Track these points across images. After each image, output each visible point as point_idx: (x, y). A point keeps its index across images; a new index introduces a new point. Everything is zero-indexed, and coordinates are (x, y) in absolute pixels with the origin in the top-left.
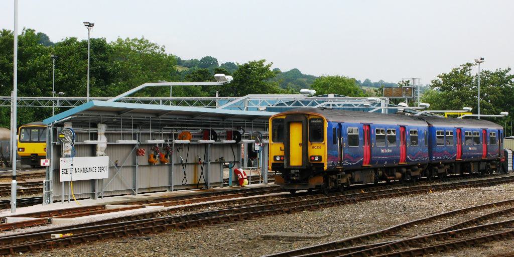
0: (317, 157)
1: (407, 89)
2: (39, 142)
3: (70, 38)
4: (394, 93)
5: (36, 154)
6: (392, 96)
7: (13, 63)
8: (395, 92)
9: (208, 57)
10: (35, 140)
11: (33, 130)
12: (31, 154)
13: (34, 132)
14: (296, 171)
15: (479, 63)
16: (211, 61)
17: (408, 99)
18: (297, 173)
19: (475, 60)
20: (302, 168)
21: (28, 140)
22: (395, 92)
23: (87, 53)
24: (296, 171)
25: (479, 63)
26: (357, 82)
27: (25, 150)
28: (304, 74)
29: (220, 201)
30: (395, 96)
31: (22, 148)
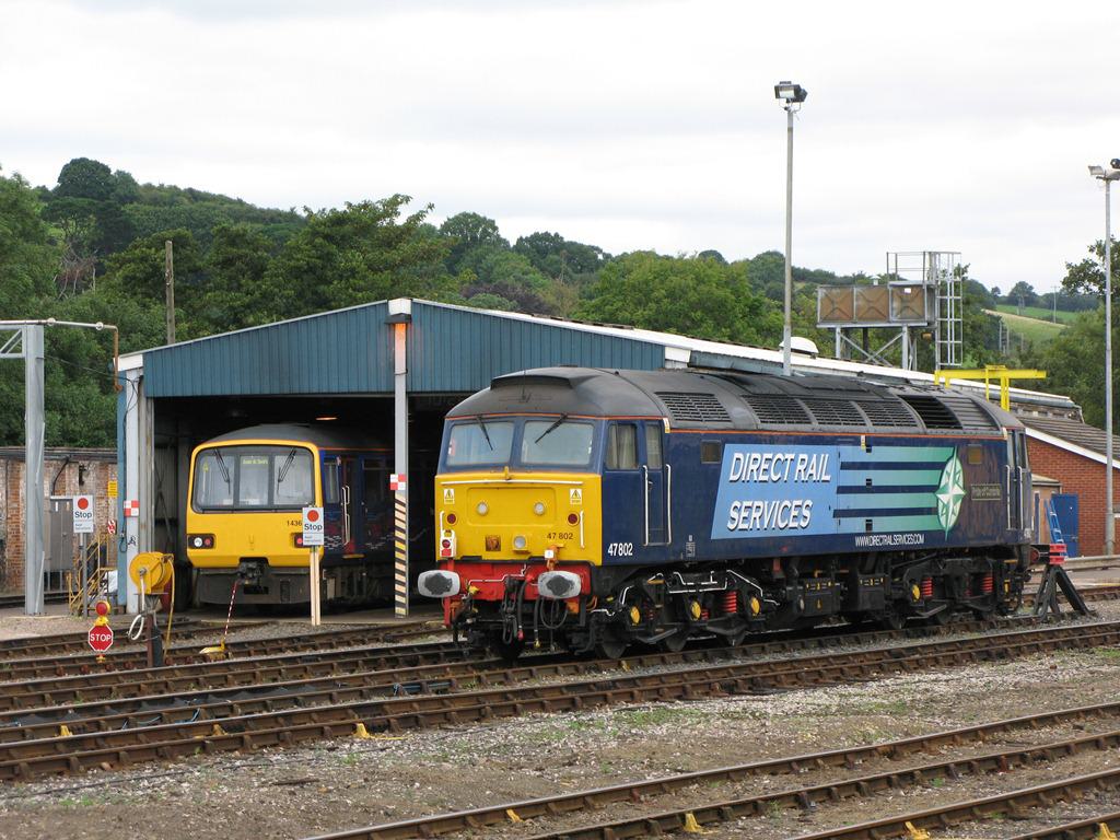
0: (200, 540)
1: (908, 290)
2: (271, 508)
3: (119, 172)
4: (859, 308)
5: (262, 561)
6: (851, 319)
7: (1020, 368)
8: (861, 303)
9: (465, 215)
10: (254, 502)
11: (246, 462)
12: (243, 560)
13: (248, 466)
14: (250, 565)
15: (1108, 179)
16: (476, 227)
17: (912, 329)
18: (252, 570)
19: (1092, 168)
20: (339, 581)
21: (228, 502)
22: (861, 303)
23: (784, 288)
24: (250, 565)
25: (1108, 179)
26: (1036, 296)
27: (217, 542)
28: (842, 275)
29: (18, 682)
30: (862, 319)
31: (204, 537)
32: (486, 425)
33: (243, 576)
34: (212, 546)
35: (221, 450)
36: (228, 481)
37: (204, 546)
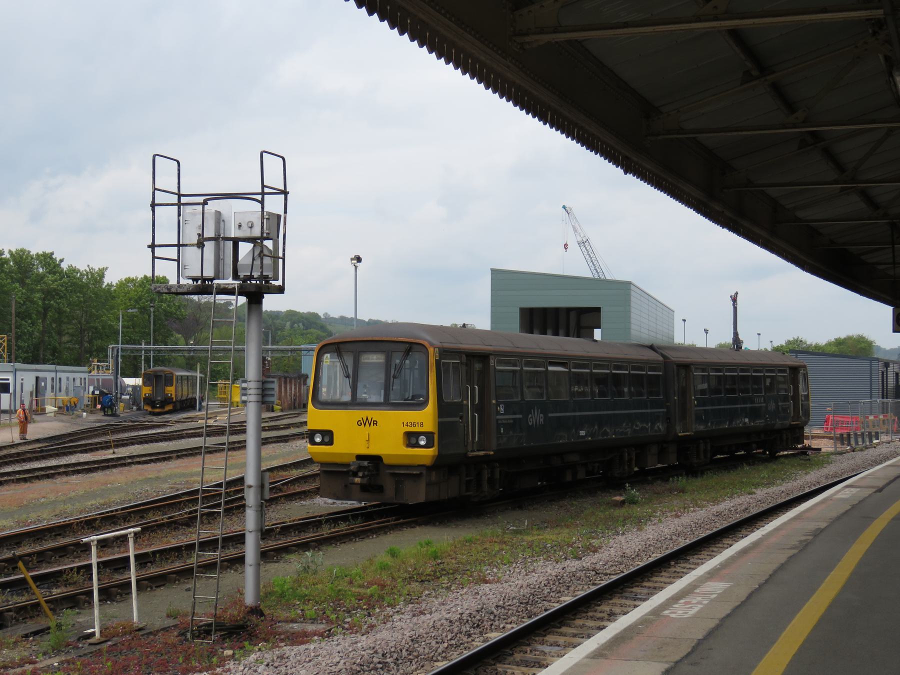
2: (387, 404)
10: (373, 399)
12: (360, 457)
21: (347, 398)
32: (402, 354)
33: (355, 474)
34: (331, 443)
35: (342, 346)
36: (348, 377)
37: (322, 443)
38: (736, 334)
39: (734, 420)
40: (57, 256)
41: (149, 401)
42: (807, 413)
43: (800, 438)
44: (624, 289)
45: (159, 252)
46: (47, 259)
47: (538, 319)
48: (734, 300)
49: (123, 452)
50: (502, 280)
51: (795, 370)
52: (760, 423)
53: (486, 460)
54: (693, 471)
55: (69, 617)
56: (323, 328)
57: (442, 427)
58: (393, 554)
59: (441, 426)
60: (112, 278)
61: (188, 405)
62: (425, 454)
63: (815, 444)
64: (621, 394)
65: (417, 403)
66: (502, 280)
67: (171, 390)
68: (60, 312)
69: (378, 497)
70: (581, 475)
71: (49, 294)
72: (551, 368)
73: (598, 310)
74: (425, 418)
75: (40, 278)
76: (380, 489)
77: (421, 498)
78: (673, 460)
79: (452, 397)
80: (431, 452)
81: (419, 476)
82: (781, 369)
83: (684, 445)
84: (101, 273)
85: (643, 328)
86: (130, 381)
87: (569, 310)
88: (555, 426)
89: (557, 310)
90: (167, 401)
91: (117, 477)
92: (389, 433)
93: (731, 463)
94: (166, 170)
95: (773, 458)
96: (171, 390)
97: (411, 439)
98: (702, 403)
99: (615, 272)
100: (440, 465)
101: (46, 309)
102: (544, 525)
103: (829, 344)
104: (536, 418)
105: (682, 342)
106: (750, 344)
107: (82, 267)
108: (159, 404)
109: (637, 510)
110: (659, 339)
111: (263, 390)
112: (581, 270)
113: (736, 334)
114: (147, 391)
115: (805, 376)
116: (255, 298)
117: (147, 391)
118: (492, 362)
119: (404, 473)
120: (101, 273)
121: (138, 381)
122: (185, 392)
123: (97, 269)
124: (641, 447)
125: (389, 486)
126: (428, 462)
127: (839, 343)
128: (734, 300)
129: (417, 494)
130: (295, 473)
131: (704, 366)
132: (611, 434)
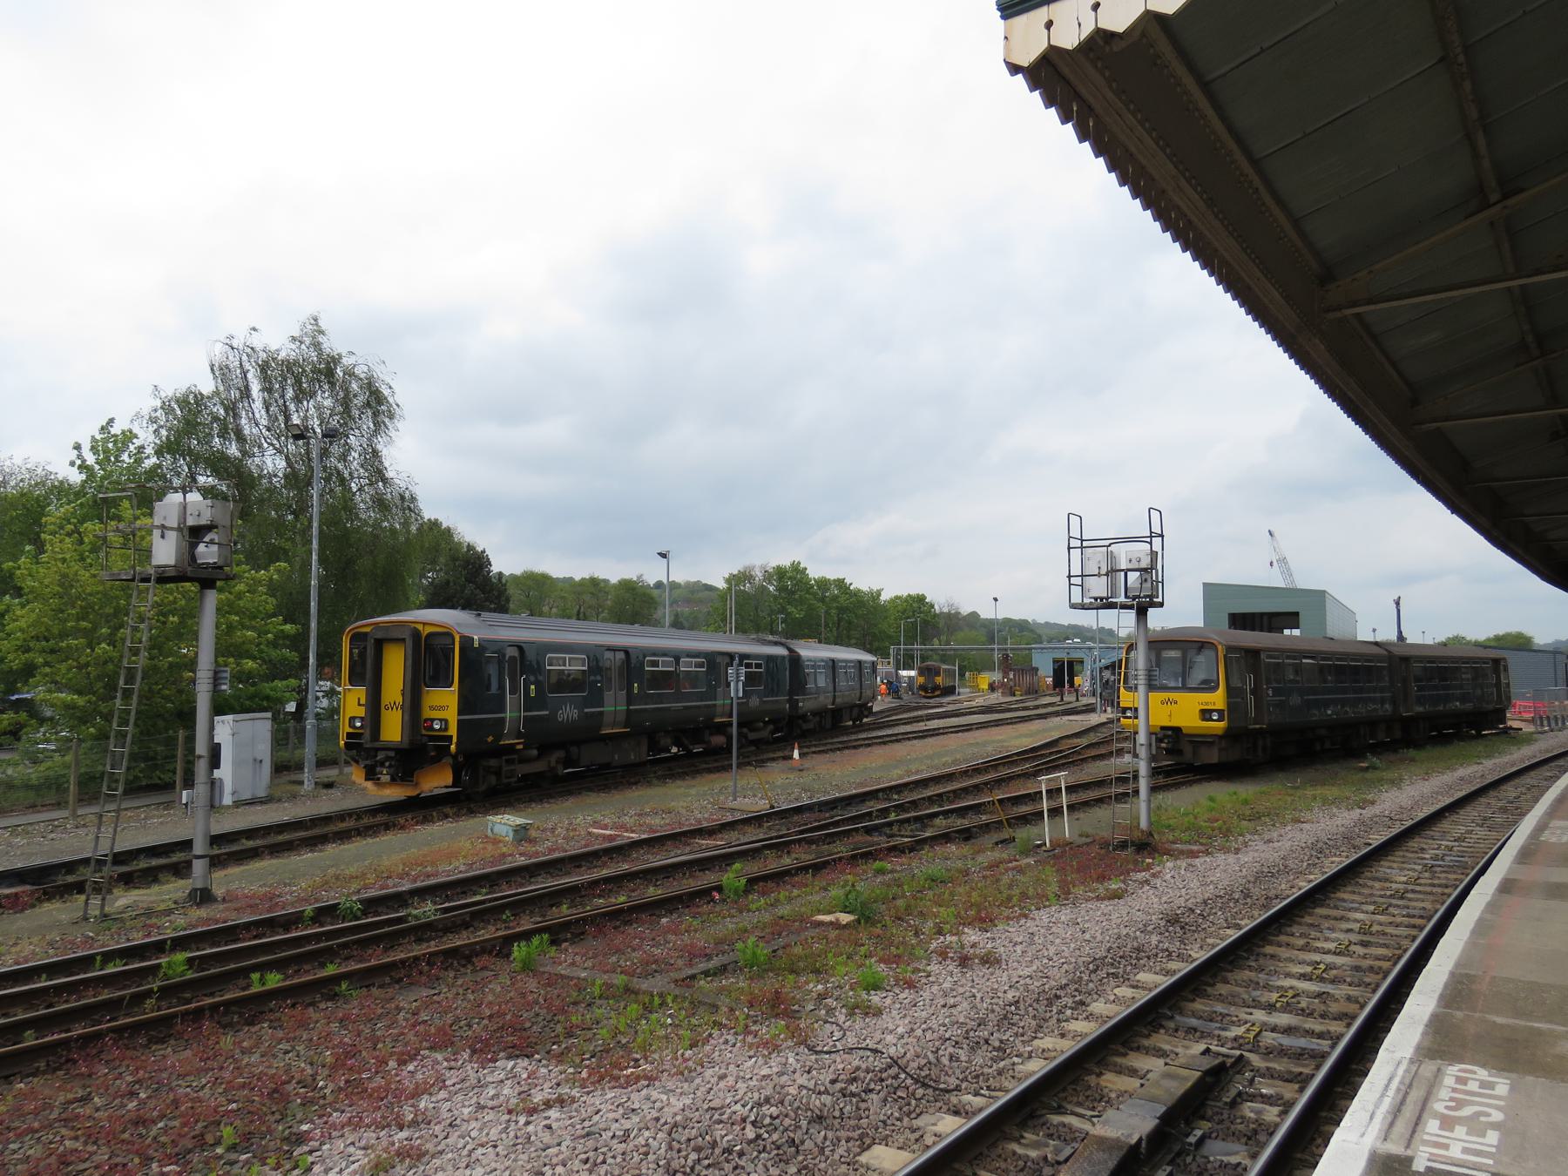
2: (1185, 688)
10: (1172, 684)
12: (1163, 728)
38: (1400, 632)
39: (1433, 703)
40: (848, 581)
41: (923, 688)
42: (1509, 699)
43: (1503, 720)
44: (1321, 595)
45: (1073, 580)
46: (840, 583)
47: (1240, 621)
48: (1397, 603)
49: (921, 726)
50: (1211, 591)
51: (1496, 662)
52: (1469, 706)
53: (1260, 732)
54: (1417, 745)
55: (1022, 833)
56: (1032, 631)
57: (1231, 706)
58: (1212, 799)
59: (1229, 704)
60: (885, 597)
61: (950, 691)
62: (1219, 726)
63: (1515, 724)
64: (1325, 681)
65: (1208, 686)
66: (1211, 591)
67: (939, 680)
68: (850, 623)
69: (1180, 758)
70: (1328, 745)
71: (842, 610)
72: (811, 651)
73: (1297, 614)
74: (1217, 699)
75: (835, 598)
76: (1180, 752)
77: (1215, 760)
78: (1398, 734)
79: (1236, 683)
80: (1222, 724)
81: (1212, 743)
82: (1484, 660)
83: (1408, 724)
84: (879, 593)
85: (1335, 628)
86: (904, 673)
87: (1262, 615)
88: (1308, 706)
89: (1253, 615)
90: (936, 688)
91: (952, 741)
92: (1187, 710)
93: (1443, 740)
94: (1075, 521)
95: (1479, 736)
96: (939, 680)
97: (1206, 714)
98: (1420, 689)
99: (1304, 582)
100: (1231, 735)
101: (839, 621)
102: (1314, 783)
103: (1488, 640)
104: (1295, 700)
105: (1388, 634)
106: (1413, 637)
107: (865, 588)
108: (932, 690)
109: (1378, 774)
110: (1348, 636)
111: (216, 673)
112: (1276, 580)
113: (1400, 632)
114: (921, 680)
115: (1506, 669)
116: (1142, 612)
117: (921, 680)
118: (1263, 656)
119: (1200, 741)
120: (879, 593)
121: (913, 673)
122: (949, 683)
123: (721, 584)
124: (1372, 723)
125: (1188, 750)
126: (1220, 732)
127: (1498, 638)
128: (1397, 603)
129: (1212, 756)
130: (1084, 741)
131: (1420, 659)
132: (1350, 713)
